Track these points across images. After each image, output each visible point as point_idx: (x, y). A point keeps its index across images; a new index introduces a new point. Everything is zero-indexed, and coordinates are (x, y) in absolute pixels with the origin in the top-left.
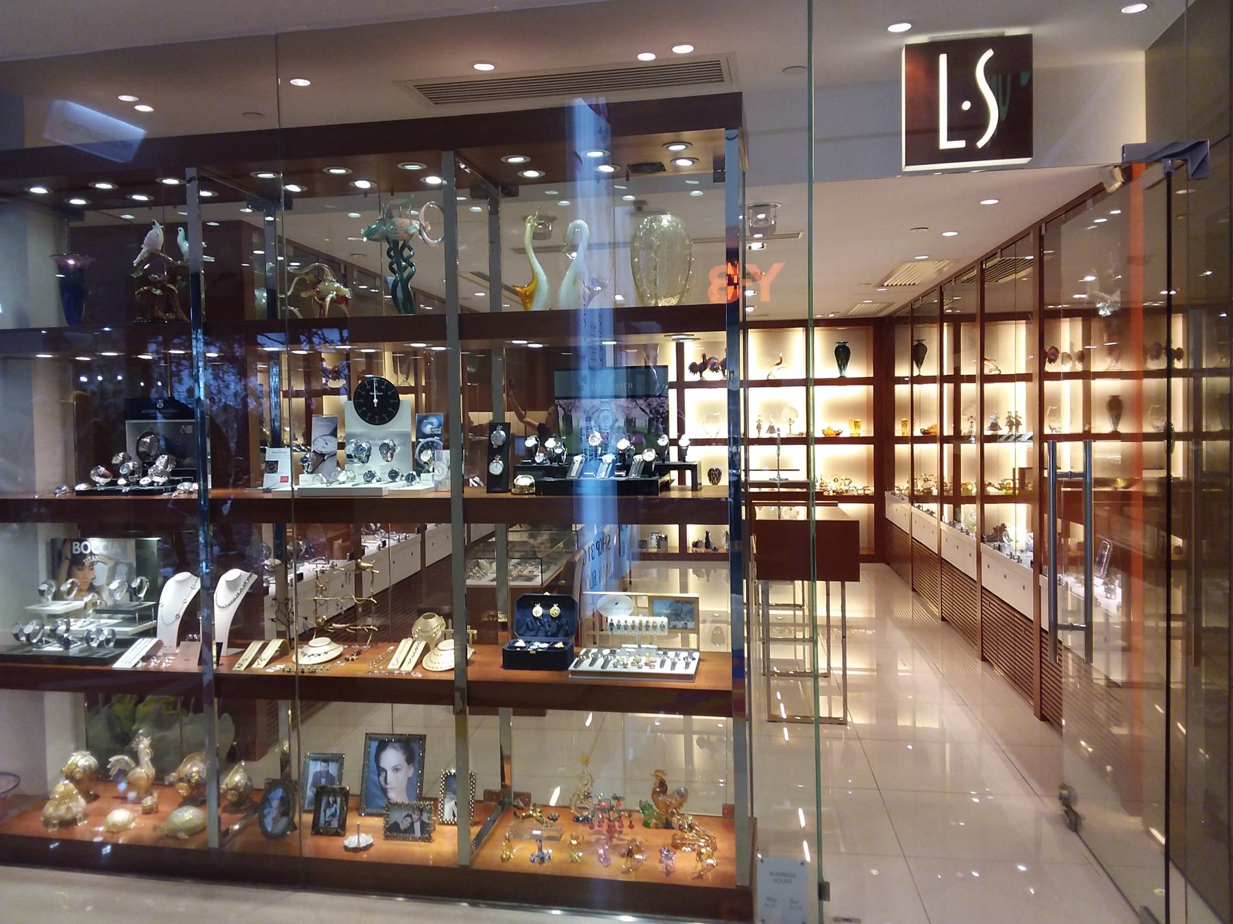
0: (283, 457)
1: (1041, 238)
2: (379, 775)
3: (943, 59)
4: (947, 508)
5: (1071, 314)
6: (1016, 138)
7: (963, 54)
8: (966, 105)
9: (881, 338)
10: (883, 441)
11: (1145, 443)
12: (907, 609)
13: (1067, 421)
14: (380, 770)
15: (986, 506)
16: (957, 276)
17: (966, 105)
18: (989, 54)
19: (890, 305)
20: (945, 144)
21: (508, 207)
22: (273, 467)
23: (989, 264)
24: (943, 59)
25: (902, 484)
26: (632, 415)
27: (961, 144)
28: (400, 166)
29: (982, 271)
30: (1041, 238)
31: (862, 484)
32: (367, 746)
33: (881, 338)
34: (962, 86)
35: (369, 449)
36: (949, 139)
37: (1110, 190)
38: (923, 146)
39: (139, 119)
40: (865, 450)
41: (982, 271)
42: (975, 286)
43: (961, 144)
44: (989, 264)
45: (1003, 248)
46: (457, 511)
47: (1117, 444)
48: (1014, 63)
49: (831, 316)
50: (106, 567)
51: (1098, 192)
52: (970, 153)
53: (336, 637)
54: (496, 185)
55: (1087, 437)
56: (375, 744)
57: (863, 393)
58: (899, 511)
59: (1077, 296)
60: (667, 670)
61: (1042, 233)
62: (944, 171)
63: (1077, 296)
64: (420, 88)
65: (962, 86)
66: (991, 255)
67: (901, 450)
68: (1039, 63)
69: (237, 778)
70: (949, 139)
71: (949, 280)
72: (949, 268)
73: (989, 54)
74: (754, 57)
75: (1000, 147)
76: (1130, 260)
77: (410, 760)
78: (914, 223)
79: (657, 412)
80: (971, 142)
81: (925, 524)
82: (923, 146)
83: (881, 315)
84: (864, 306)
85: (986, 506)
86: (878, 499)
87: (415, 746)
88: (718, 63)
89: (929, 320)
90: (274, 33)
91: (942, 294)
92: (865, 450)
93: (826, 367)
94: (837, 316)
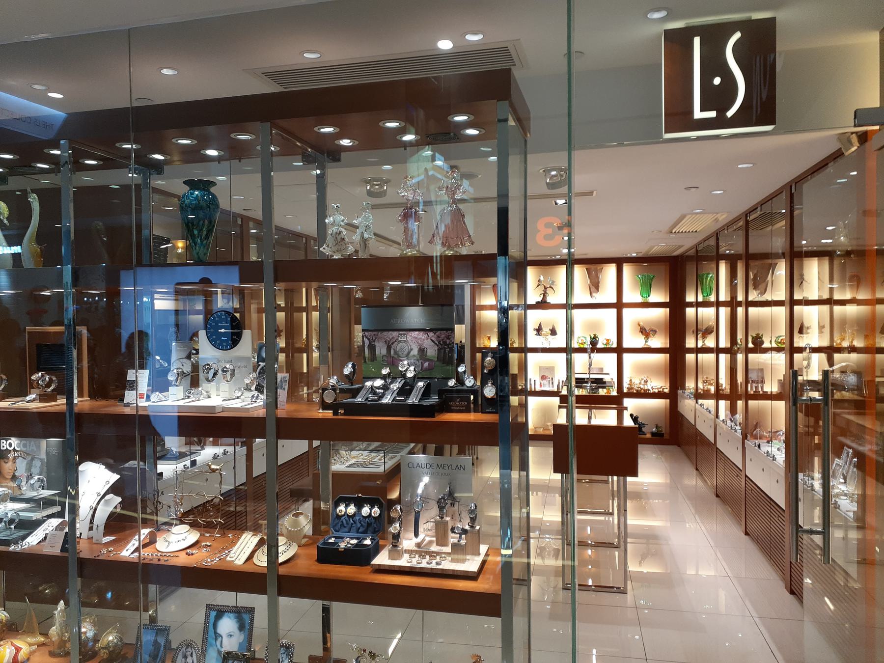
0: (143, 378)
1: (792, 195)
2: (216, 639)
3: (697, 41)
4: (723, 404)
5: (819, 254)
6: (762, 110)
7: (714, 37)
8: (717, 81)
9: (675, 270)
10: (676, 351)
11: (877, 355)
12: (692, 480)
13: (813, 338)
14: (217, 636)
15: (750, 402)
16: (728, 225)
17: (717, 81)
18: (737, 35)
19: (680, 247)
20: (698, 114)
21: (334, 173)
22: (133, 385)
23: (752, 217)
24: (697, 41)
25: (690, 384)
26: (425, 346)
27: (712, 114)
28: (232, 136)
29: (747, 222)
30: (792, 195)
31: (659, 383)
32: (207, 616)
33: (675, 270)
34: (714, 63)
35: (233, 371)
36: (703, 109)
37: (846, 154)
38: (680, 118)
39: (52, 103)
40: (663, 358)
41: (748, 222)
42: (742, 233)
43: (712, 114)
44: (752, 217)
45: (762, 203)
46: (271, 428)
47: (854, 356)
48: (760, 43)
49: (634, 255)
50: (25, 462)
51: (837, 155)
52: (720, 122)
53: (194, 525)
54: (322, 153)
55: (830, 351)
56: (213, 614)
57: (662, 313)
58: (687, 405)
59: (824, 241)
60: (433, 565)
61: (791, 192)
62: (699, 138)
63: (824, 241)
64: (267, 74)
65: (714, 63)
66: (753, 209)
67: (690, 357)
68: (782, 46)
69: (111, 638)
70: (703, 109)
71: (722, 229)
72: (724, 218)
73: (737, 35)
74: (534, 45)
75: (743, 118)
76: (866, 213)
77: (241, 628)
78: (696, 182)
79: (445, 343)
80: (722, 111)
81: (706, 414)
82: (680, 118)
83: (675, 254)
84: (659, 247)
85: (750, 402)
86: (673, 395)
87: (246, 617)
88: (506, 50)
89: (708, 259)
90: (127, 28)
91: (718, 239)
92: (663, 358)
93: (631, 294)
94: (640, 255)
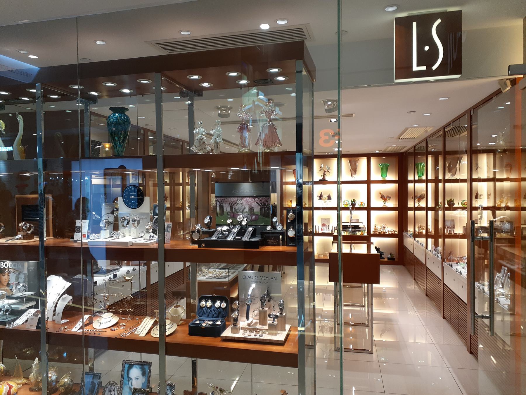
0: (85, 225)
1: (471, 116)
2: (129, 381)
3: (415, 24)
4: (430, 241)
5: (487, 151)
6: (453, 65)
7: (425, 22)
8: (427, 48)
9: (402, 161)
10: (402, 209)
11: (522, 212)
12: (412, 286)
13: (484, 201)
14: (129, 379)
15: (446, 239)
16: (433, 134)
17: (427, 48)
18: (439, 21)
19: (405, 147)
20: (415, 68)
21: (199, 103)
22: (79, 229)
23: (448, 129)
24: (415, 24)
25: (411, 229)
26: (253, 206)
27: (424, 68)
28: (138, 81)
29: (445, 132)
30: (471, 116)
31: (392, 228)
32: (123, 367)
33: (402, 161)
34: (425, 38)
35: (139, 221)
36: (418, 65)
37: (504, 92)
38: (405, 70)
39: (31, 61)
40: (394, 213)
41: (445, 132)
42: (441, 139)
43: (424, 68)
44: (448, 129)
45: (454, 121)
46: (161, 255)
47: (508, 212)
48: (452, 26)
49: (377, 152)
50: (15, 275)
51: (498, 92)
52: (429, 73)
53: (115, 313)
54: (192, 91)
55: (494, 209)
56: (127, 366)
57: (394, 187)
58: (409, 242)
59: (490, 144)
60: (258, 337)
61: (471, 114)
62: (416, 82)
63: (490, 144)
64: (159, 44)
65: (425, 38)
66: (448, 125)
67: (411, 213)
68: (465, 27)
69: (66, 380)
70: (418, 65)
71: (430, 136)
72: (431, 130)
73: (439, 21)
74: (318, 27)
75: (442, 70)
76: (515, 127)
77: (144, 374)
78: (414, 108)
79: (265, 204)
80: (429, 66)
81: (420, 247)
82: (405, 70)
83: (402, 151)
84: (392, 147)
85: (446, 239)
86: (400, 235)
87: (147, 368)
88: (301, 30)
89: (421, 154)
90: (76, 16)
91: (427, 142)
92: (394, 213)
93: (376, 175)
94: (381, 152)
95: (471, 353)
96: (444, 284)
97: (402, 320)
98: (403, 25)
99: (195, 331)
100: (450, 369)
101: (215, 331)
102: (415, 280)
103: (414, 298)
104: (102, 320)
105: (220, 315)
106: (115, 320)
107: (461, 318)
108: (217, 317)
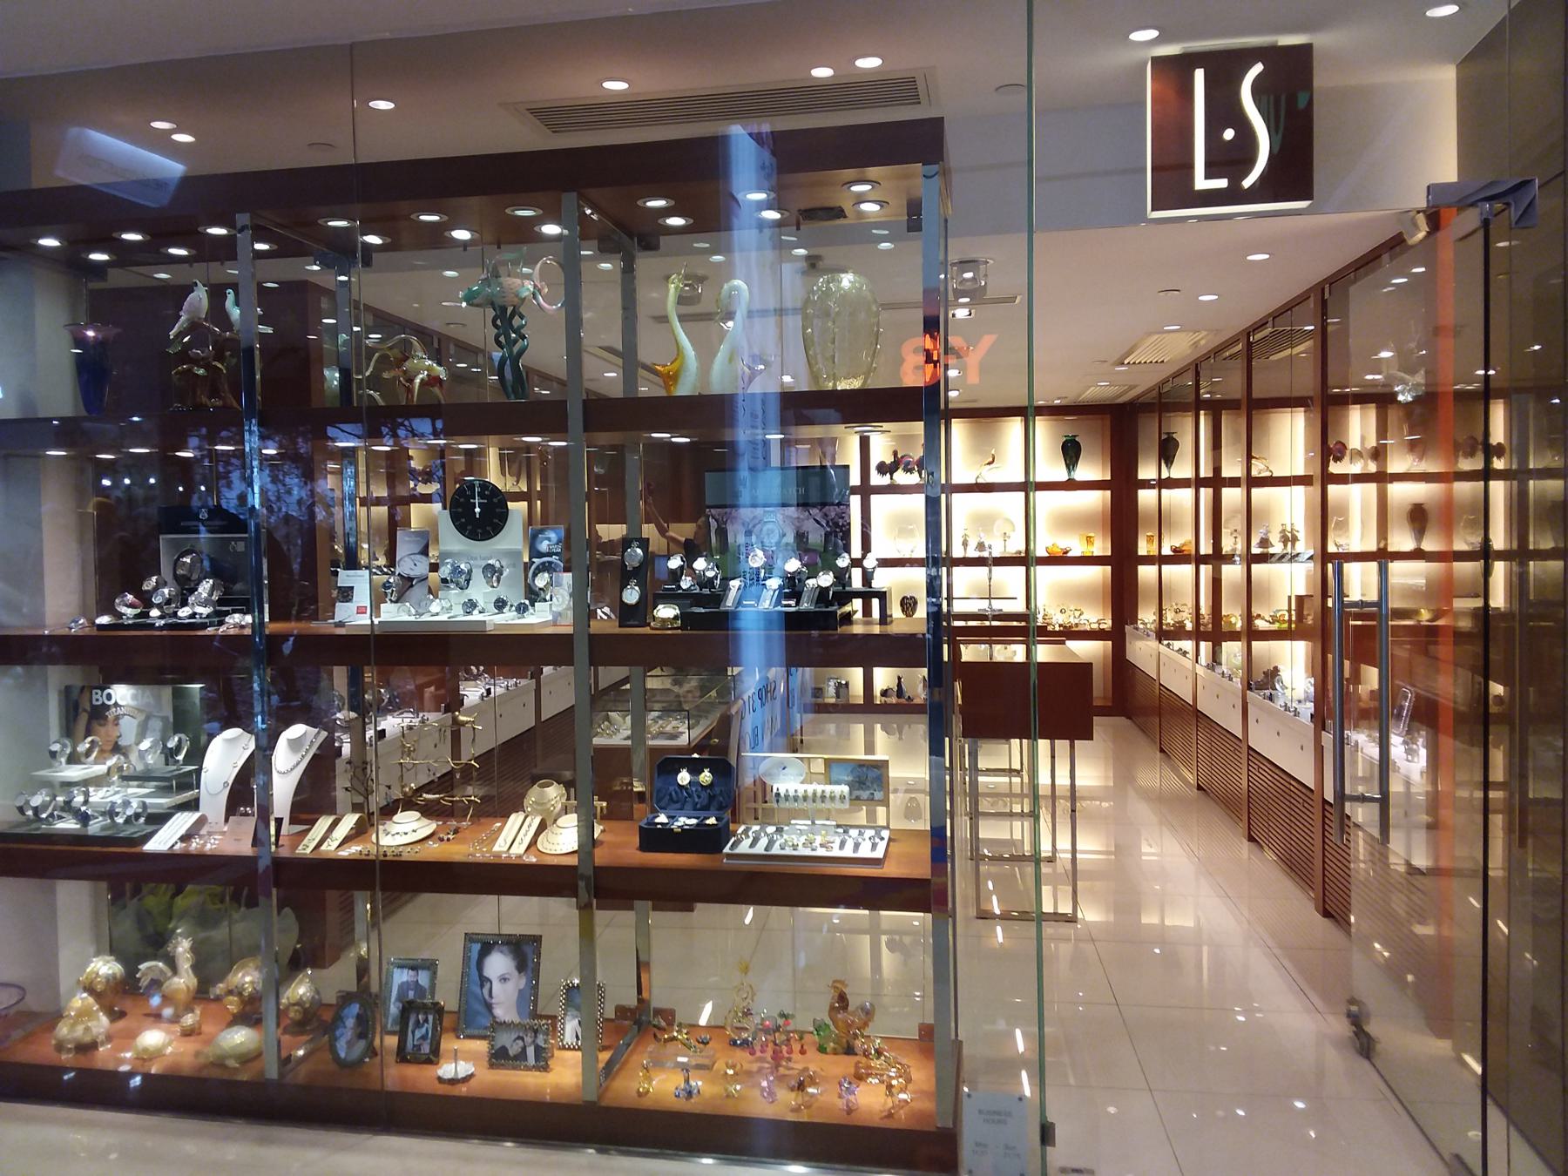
0: (359, 582)
1: (1324, 303)
2: (482, 986)
3: (1199, 75)
4: (1205, 647)
5: (1361, 399)
6: (1292, 175)
7: (1225, 69)
8: (1229, 134)
9: (1120, 430)
10: (1123, 561)
11: (1456, 564)
12: (1154, 775)
13: (1357, 536)
14: (484, 980)
15: (1254, 644)
16: (1217, 351)
17: (1229, 134)
18: (1258, 68)
19: (1132, 388)
20: (1201, 183)
21: (645, 264)
22: (347, 594)
23: (1258, 336)
24: (1199, 75)
25: (1147, 616)
26: (804, 529)
27: (1222, 183)
28: (508, 211)
29: (1249, 345)
30: (1324, 303)
31: (1096, 616)
32: (466, 950)
33: (1120, 430)
34: (1224, 110)
35: (470, 572)
36: (1207, 177)
37: (1411, 241)
38: (1174, 186)
39: (176, 151)
40: (1100, 573)
41: (1249, 345)
42: (1240, 364)
43: (1222, 183)
44: (1258, 336)
45: (1276, 315)
46: (581, 650)
47: (1420, 566)
48: (1290, 80)
49: (1057, 402)
50: (135, 722)
51: (1396, 244)
52: (1233, 195)
53: (428, 811)
54: (631, 235)
55: (1383, 556)
56: (476, 947)
57: (1098, 500)
58: (1143, 651)
59: (1369, 377)
60: (848, 852)
61: (1326, 297)
62: (1200, 218)
63: (1369, 377)
64: (534, 112)
65: (1224, 110)
66: (1261, 325)
67: (1146, 573)
68: (1322, 80)
69: (301, 991)
70: (1207, 177)
71: (1206, 357)
72: (1206, 341)
73: (1258, 68)
74: (959, 73)
75: (1271, 188)
76: (1437, 331)
77: (521, 967)
78: (1163, 284)
79: (836, 524)
80: (1235, 180)
81: (1176, 667)
82: (1174, 186)
83: (1120, 400)
84: (1099, 389)
85: (1254, 644)
86: (1116, 635)
87: (528, 949)
88: (913, 81)
89: (1181, 407)
90: (348, 42)
91: (1197, 374)
92: (1100, 573)
93: (1050, 467)
94: (1065, 402)
95: (1326, 914)
96: (1250, 748)
97: (1124, 862)
98: (1175, 71)
99: (654, 839)
100: (1277, 951)
101: (709, 840)
102: (1162, 751)
103: (1162, 800)
104: (393, 828)
105: (715, 803)
106: (427, 827)
107: (1298, 831)
108: (706, 808)
